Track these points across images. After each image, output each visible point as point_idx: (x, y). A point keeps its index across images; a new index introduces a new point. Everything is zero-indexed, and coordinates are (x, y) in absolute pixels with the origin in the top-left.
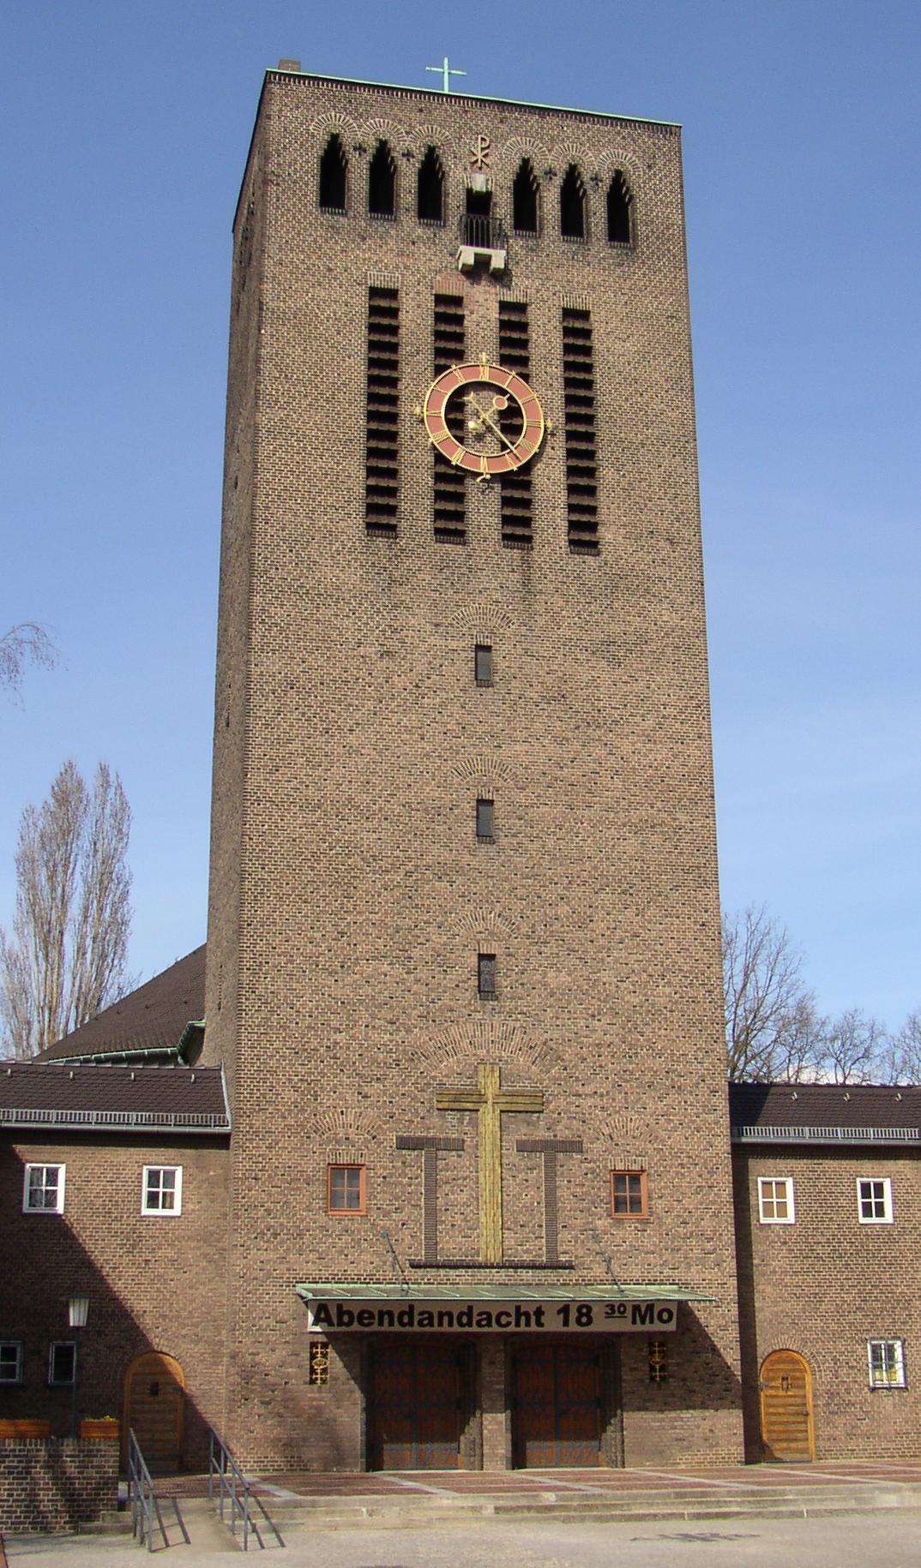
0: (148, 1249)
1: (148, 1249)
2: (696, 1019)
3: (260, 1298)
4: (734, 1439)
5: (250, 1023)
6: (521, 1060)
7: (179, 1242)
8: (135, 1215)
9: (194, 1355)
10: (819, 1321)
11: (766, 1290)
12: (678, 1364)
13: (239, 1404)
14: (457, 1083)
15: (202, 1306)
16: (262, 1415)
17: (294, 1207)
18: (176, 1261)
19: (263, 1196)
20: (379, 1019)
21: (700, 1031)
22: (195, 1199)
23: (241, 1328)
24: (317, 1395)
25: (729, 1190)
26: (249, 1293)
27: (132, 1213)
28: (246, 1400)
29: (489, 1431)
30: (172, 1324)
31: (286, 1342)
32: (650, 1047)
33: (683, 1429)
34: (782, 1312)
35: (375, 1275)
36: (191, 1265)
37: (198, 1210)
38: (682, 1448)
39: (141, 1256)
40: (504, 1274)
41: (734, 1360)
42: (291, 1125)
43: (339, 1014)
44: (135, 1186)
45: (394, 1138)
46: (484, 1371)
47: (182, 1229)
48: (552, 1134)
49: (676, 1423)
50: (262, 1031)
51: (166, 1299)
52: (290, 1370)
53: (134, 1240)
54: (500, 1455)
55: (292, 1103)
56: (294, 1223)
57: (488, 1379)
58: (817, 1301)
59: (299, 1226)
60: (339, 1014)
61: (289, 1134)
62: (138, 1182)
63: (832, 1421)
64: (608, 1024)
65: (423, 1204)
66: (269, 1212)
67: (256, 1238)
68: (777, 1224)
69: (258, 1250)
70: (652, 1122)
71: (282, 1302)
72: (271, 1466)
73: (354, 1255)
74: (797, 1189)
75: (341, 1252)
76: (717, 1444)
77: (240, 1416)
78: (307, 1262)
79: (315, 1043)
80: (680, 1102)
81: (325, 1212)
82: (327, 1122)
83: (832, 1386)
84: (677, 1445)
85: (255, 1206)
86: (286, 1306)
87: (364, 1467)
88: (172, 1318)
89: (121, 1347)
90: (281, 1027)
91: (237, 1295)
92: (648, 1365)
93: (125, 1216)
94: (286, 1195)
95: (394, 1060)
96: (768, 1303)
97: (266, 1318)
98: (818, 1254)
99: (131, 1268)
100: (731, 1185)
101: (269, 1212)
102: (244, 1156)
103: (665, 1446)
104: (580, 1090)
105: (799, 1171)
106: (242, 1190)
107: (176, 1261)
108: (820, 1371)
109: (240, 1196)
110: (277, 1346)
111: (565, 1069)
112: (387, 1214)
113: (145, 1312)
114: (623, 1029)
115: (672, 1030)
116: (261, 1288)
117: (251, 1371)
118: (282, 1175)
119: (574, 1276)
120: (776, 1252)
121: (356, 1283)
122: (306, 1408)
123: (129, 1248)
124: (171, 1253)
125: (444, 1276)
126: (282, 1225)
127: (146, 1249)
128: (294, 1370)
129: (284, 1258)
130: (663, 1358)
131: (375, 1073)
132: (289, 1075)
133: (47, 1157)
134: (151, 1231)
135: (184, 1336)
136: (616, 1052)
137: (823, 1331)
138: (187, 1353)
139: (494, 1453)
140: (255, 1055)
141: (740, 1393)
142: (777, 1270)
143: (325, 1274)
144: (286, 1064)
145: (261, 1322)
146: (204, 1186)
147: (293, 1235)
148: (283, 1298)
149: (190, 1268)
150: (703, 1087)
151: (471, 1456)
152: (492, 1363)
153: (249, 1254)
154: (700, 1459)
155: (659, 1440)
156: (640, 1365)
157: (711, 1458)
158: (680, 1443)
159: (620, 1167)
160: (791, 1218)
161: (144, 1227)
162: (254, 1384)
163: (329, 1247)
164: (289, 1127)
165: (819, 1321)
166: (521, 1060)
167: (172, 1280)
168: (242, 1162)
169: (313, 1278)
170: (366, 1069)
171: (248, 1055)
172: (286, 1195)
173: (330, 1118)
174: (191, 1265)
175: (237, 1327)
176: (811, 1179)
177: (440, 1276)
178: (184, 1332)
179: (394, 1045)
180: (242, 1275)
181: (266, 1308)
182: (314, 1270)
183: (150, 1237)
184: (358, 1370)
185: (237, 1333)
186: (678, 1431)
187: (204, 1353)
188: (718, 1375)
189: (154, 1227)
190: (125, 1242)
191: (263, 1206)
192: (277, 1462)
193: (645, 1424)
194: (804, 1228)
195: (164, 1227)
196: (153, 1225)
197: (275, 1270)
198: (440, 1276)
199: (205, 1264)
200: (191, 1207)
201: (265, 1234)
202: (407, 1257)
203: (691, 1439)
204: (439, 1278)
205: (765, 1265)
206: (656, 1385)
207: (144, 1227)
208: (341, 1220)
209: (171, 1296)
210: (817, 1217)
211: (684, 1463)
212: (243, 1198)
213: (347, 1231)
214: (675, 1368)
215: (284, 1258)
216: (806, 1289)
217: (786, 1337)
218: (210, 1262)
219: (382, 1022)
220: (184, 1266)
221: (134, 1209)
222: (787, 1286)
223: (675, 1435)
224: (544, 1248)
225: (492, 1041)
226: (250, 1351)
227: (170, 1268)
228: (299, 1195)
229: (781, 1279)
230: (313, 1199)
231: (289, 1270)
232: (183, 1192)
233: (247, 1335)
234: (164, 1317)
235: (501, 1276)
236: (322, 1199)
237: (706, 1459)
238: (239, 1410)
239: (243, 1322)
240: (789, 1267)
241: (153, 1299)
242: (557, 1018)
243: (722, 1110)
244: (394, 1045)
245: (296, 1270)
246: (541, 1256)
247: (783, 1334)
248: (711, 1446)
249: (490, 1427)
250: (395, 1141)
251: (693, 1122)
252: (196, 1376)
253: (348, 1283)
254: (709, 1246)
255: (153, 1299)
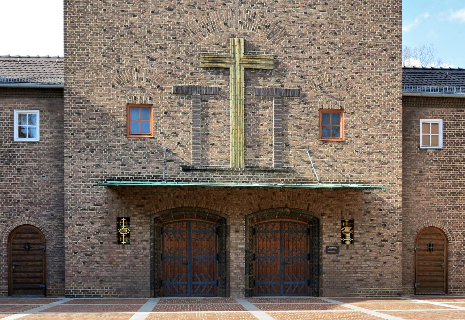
0: (19, 162)
1: (19, 162)
2: (382, 9)
3: (83, 190)
4: (395, 280)
5: (72, 10)
6: (259, 35)
7: (39, 157)
8: (9, 141)
9: (51, 227)
10: (455, 210)
11: (422, 191)
12: (360, 234)
13: (71, 256)
14: (213, 50)
15: (55, 197)
16: (86, 262)
17: (104, 132)
18: (37, 169)
19: (84, 125)
20: (161, 7)
21: (384, 16)
22: (48, 131)
23: (71, 209)
24: (122, 251)
25: (400, 123)
26: (76, 187)
27: (8, 140)
28: (75, 253)
29: (235, 273)
30: (36, 208)
31: (101, 218)
32: (350, 27)
33: (362, 274)
34: (432, 204)
35: (160, 176)
36: (47, 172)
37: (51, 138)
38: (361, 285)
39: (15, 167)
40: (245, 176)
41: (398, 232)
42: (102, 79)
43: (134, 4)
44: (9, 123)
45: (172, 87)
46: (232, 236)
47: (41, 150)
48: (280, 85)
49: (357, 270)
50: (81, 16)
51: (32, 193)
52: (104, 235)
53: (10, 157)
54: (242, 288)
55: (102, 64)
56: (104, 142)
57: (234, 241)
58: (455, 198)
59: (108, 144)
60: (134, 4)
61: (101, 85)
62: (11, 120)
63: (459, 271)
64: (321, 11)
65: (191, 131)
66: (88, 135)
67: (79, 152)
68: (431, 149)
69: (81, 159)
70: (349, 78)
71: (98, 193)
72: (92, 293)
73: (145, 163)
74: (445, 127)
75: (136, 161)
76: (384, 283)
77: (72, 263)
78: (114, 168)
79: (116, 24)
80: (368, 64)
81: (126, 135)
82: (126, 76)
83: (461, 250)
84: (358, 284)
85: (78, 131)
86: (100, 195)
87: (153, 294)
88: (36, 204)
89: (4, 222)
90: (93, 13)
91: (68, 188)
92: (341, 234)
93: (4, 141)
94: (99, 124)
95: (171, 35)
96: (422, 198)
97: (88, 203)
98: (458, 168)
99: (9, 174)
100: (401, 120)
101: (88, 135)
102: (70, 99)
103: (350, 284)
104: (301, 56)
105: (448, 116)
106: (69, 121)
107: (37, 169)
108: (454, 240)
109: (68, 125)
110: (95, 220)
111: (289, 42)
112: (168, 138)
113: (19, 201)
114: (331, 15)
115: (365, 15)
116: (84, 184)
117: (78, 236)
118: (96, 111)
119: (293, 177)
120: (429, 167)
121: (147, 181)
122: (115, 258)
123: (7, 162)
124: (34, 165)
125: (206, 176)
126: (96, 143)
127: (18, 162)
128: (107, 235)
129: (98, 165)
130: (350, 230)
131: (159, 43)
132: (100, 45)
133: (426, 292)
134: (20, 151)
135: (44, 216)
136: (325, 30)
137: (458, 216)
138: (47, 225)
139: (237, 286)
140: (76, 32)
141: (401, 252)
142: (430, 177)
143: (126, 175)
144: (98, 38)
145: (84, 205)
146: (54, 123)
147: (104, 150)
148: (98, 190)
149: (47, 174)
150: (385, 55)
151: (223, 288)
152: (237, 232)
153: (75, 162)
154: (373, 292)
155: (345, 280)
156: (335, 234)
157: (379, 292)
158: (360, 282)
159: (326, 107)
160: (441, 145)
161: (16, 148)
162: (81, 244)
163: (128, 158)
164: (100, 80)
165: (455, 210)
166: (259, 35)
167: (35, 181)
168: (69, 103)
169: (118, 178)
170: (152, 41)
171: (71, 32)
172: (99, 124)
173: (128, 74)
174: (47, 172)
175: (69, 209)
176: (456, 120)
177: (203, 176)
178: (44, 213)
179: (172, 25)
180: (70, 175)
181: (86, 196)
182: (119, 173)
183: (20, 155)
184: (149, 235)
185: (68, 212)
186: (359, 275)
187: (57, 226)
188: (387, 241)
189: (22, 149)
190: (4, 158)
191: (84, 131)
192: (97, 291)
193: (337, 271)
194: (449, 152)
195: (29, 148)
196: (22, 147)
197: (92, 172)
198: (203, 176)
199: (56, 171)
200: (46, 136)
201: (85, 149)
202: (180, 164)
203: (367, 280)
204: (202, 178)
205: (422, 175)
206: (345, 246)
207: (16, 148)
208: (137, 140)
209: (35, 191)
210: (458, 145)
211: (362, 295)
212: (70, 126)
213: (141, 148)
214: (359, 236)
215: (98, 165)
216: (448, 190)
217: (433, 219)
218: (60, 170)
219: (163, 9)
220: (43, 173)
221: (9, 137)
222: (436, 188)
223: (357, 278)
224: (273, 159)
225: (240, 22)
226: (77, 223)
227: (34, 174)
228: (108, 125)
229: (432, 184)
230: (117, 127)
231: (102, 172)
232: (40, 127)
233: (75, 213)
234: (31, 204)
235: (244, 177)
236: (123, 127)
237: (377, 292)
238: (71, 259)
239: (72, 205)
240: (437, 176)
241: (24, 193)
242: (285, 7)
243: (398, 70)
244: (172, 25)
245: (107, 173)
246: (271, 164)
247: (431, 217)
248: (380, 284)
249: (235, 271)
250: (172, 89)
251: (377, 78)
252: (53, 240)
253: (141, 181)
254: (384, 160)
255: (24, 193)
